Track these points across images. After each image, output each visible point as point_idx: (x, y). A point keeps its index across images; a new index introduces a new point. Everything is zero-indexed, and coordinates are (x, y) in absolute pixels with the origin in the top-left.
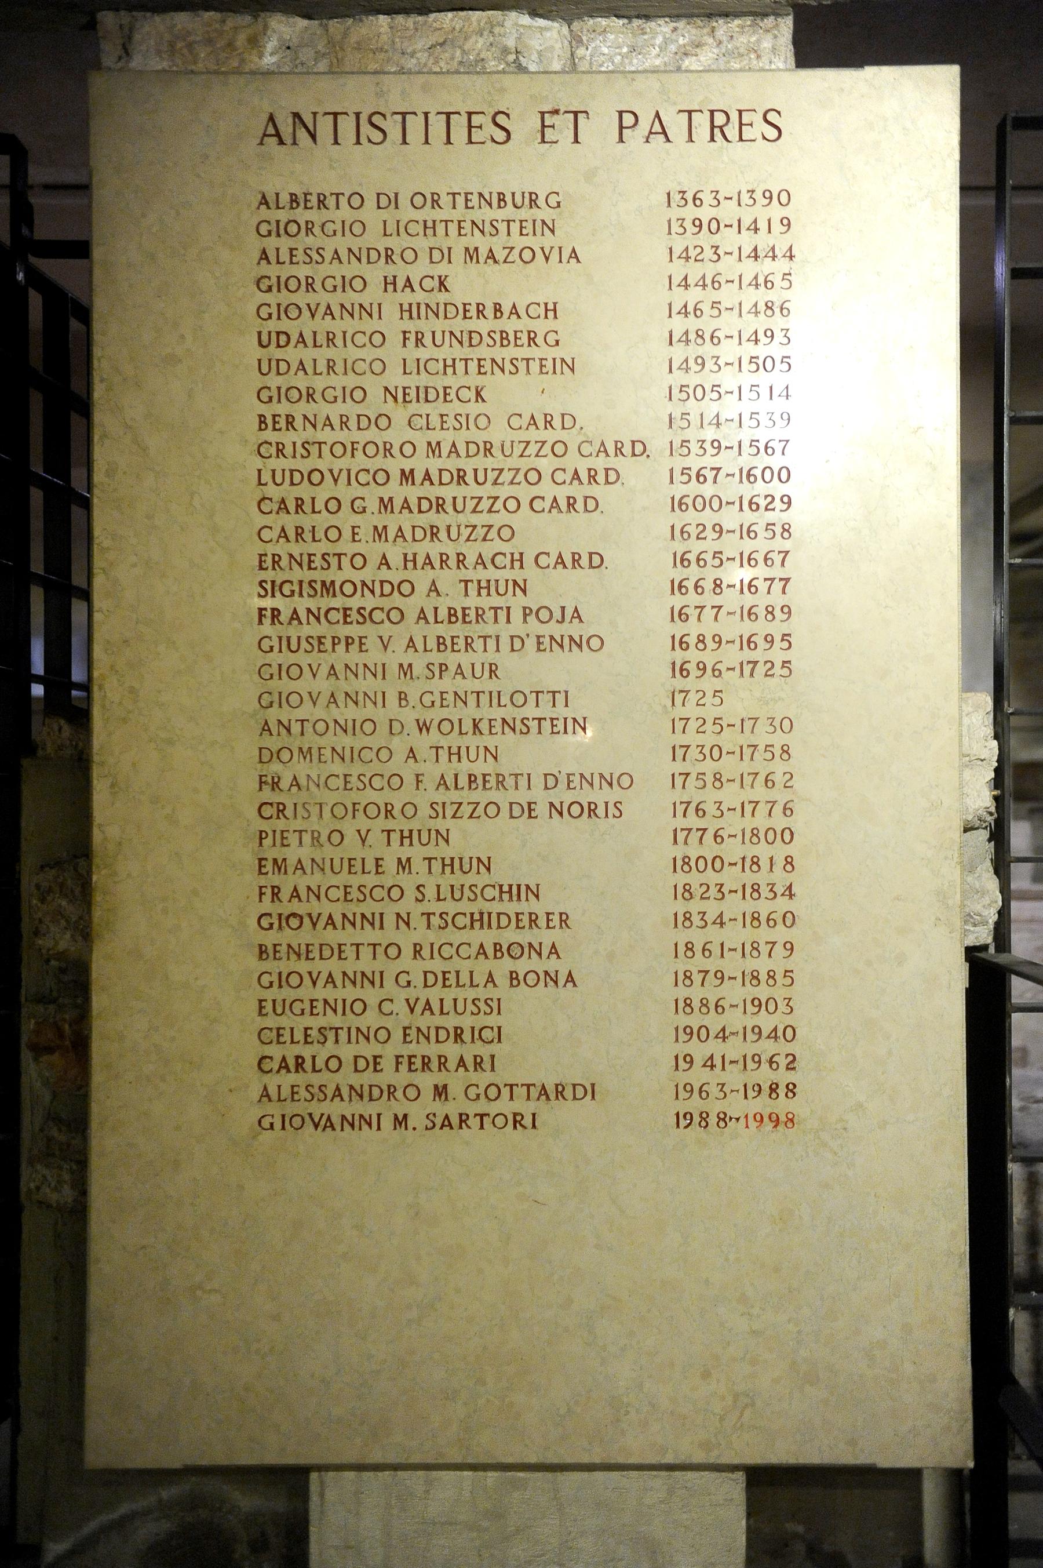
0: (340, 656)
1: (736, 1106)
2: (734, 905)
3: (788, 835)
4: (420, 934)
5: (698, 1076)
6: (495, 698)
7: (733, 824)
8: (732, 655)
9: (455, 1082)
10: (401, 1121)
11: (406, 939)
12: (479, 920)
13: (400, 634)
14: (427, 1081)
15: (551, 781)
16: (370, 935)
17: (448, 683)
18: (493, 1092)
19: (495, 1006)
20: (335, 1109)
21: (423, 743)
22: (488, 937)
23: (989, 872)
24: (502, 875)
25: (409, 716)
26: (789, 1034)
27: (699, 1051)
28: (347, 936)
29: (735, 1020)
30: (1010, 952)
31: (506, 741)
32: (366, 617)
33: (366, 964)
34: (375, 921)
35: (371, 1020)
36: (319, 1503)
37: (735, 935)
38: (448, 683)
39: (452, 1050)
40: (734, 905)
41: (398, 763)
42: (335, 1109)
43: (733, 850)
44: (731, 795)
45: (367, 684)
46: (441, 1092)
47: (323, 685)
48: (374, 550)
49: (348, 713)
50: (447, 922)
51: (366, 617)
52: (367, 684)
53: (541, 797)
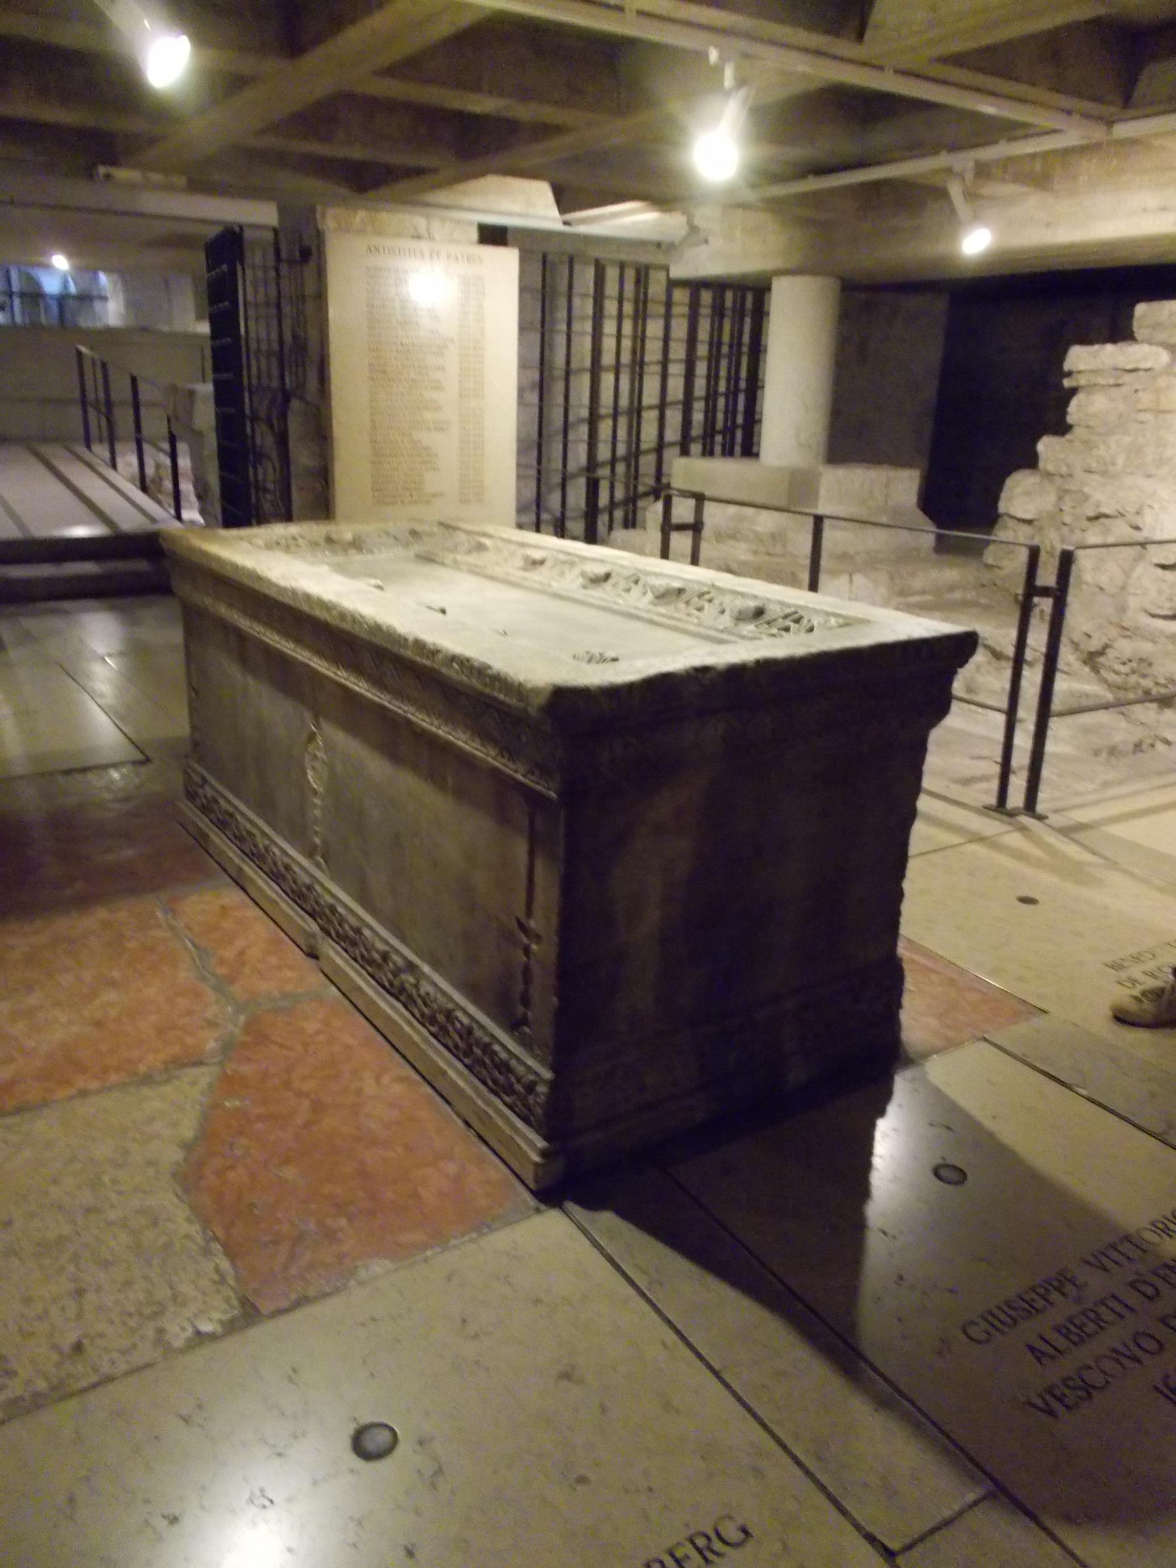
30: (750, 450)
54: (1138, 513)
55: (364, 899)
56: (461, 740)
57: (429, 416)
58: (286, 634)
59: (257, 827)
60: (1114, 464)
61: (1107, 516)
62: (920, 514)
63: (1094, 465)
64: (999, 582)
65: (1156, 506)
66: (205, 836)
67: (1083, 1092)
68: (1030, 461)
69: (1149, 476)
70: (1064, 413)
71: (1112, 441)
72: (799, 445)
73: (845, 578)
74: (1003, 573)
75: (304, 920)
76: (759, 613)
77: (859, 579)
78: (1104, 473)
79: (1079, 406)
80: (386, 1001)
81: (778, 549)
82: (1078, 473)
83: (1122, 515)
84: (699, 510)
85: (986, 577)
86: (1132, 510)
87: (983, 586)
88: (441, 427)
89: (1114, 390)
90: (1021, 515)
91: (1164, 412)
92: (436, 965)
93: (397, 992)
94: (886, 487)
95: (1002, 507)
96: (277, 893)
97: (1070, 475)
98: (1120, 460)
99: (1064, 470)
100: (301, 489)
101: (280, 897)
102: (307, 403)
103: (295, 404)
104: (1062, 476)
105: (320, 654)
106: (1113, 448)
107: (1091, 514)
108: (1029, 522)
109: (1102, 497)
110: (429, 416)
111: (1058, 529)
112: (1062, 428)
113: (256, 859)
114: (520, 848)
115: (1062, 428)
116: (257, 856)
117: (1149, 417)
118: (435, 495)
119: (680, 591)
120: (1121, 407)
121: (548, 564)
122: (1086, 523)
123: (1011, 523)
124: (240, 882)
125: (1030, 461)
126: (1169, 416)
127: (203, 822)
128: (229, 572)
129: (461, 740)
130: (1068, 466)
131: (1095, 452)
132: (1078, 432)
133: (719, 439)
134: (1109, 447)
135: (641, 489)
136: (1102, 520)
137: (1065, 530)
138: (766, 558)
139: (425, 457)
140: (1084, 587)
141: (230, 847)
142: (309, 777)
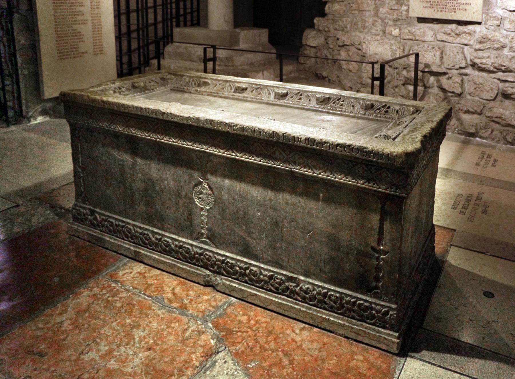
0: (61, 7)
1: (98, 52)
2: (97, 32)
3: (101, 25)
4: (71, 38)
5: (95, 50)
6: (76, 12)
7: (97, 24)
8: (96, 7)
9: (75, 53)
10: (71, 58)
11: (70, 38)
12: (76, 36)
13: (67, 5)
14: (72, 53)
15: (81, 20)
16: (66, 38)
17: (72, 10)
18: (78, 54)
19: (77, 45)
20: (65, 57)
21: (70, 17)
22: (76, 37)
23: (422, 14)
24: (78, 31)
25: (68, 14)
26: (102, 45)
27: (95, 47)
28: (64, 38)
29: (98, 44)
30: (206, 25)
31: (77, 16)
32: (63, 3)
33: (66, 41)
34: (66, 37)
35: (67, 47)
36: (3, 132)
37: (97, 35)
38: (72, 10)
39: (74, 50)
40: (97, 32)
41: (67, 19)
42: (65, 57)
43: (97, 27)
44: (96, 21)
45: (64, 11)
46: (74, 54)
47: (60, 11)
48: (68, 29)
49: (62, 14)
50: (73, 36)
51: (63, 3)
52: (64, 11)
53: (80, 22)
54: (359, 44)
55: (247, 252)
56: (338, 178)
57: (79, 18)
58: (194, 141)
59: (146, 230)
60: (346, 28)
61: (347, 45)
62: (269, 44)
63: (338, 28)
64: (307, 69)
65: (367, 42)
66: (102, 240)
67: (489, 254)
68: (312, 26)
69: (361, 32)
70: (324, 10)
71: (344, 20)
72: (226, 21)
73: (261, 73)
74: (308, 66)
75: (199, 270)
76: (372, 106)
77: (265, 73)
78: (343, 30)
79: (329, 8)
80: (276, 297)
81: (230, 64)
82: (332, 30)
83: (353, 45)
84: (214, 53)
85: (301, 67)
86: (357, 44)
87: (300, 70)
88: (84, 22)
89: (341, 3)
90: (312, 45)
91: (362, 11)
92: (307, 274)
93: (292, 294)
94: (259, 36)
95: (304, 42)
96: (170, 260)
97: (329, 31)
98: (349, 27)
99: (326, 29)
100: (21, 55)
101: (176, 262)
102: (21, 14)
103: (16, 16)
104: (325, 31)
105: (217, 147)
106: (346, 21)
107: (341, 44)
108: (315, 47)
109: (344, 39)
110: (79, 18)
111: (328, 50)
112: (323, 15)
113: (148, 246)
114: (375, 219)
115: (323, 15)
116: (147, 243)
117: (356, 12)
118: (83, 53)
119: (329, 98)
120: (344, 8)
121: (249, 89)
122: (339, 48)
123: (308, 48)
124: (137, 258)
125: (312, 26)
126: (364, 12)
127: (95, 232)
128: (132, 111)
129: (338, 178)
130: (328, 28)
131: (338, 23)
132: (330, 16)
133: (174, 20)
134: (343, 22)
135: (150, 41)
136: (345, 47)
137: (331, 50)
138: (225, 68)
139: (79, 36)
140: (343, 70)
141: (124, 243)
142: (196, 202)
